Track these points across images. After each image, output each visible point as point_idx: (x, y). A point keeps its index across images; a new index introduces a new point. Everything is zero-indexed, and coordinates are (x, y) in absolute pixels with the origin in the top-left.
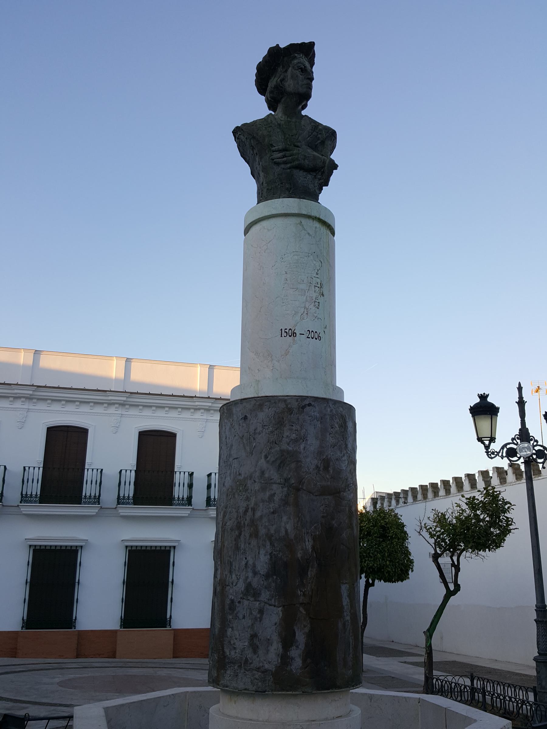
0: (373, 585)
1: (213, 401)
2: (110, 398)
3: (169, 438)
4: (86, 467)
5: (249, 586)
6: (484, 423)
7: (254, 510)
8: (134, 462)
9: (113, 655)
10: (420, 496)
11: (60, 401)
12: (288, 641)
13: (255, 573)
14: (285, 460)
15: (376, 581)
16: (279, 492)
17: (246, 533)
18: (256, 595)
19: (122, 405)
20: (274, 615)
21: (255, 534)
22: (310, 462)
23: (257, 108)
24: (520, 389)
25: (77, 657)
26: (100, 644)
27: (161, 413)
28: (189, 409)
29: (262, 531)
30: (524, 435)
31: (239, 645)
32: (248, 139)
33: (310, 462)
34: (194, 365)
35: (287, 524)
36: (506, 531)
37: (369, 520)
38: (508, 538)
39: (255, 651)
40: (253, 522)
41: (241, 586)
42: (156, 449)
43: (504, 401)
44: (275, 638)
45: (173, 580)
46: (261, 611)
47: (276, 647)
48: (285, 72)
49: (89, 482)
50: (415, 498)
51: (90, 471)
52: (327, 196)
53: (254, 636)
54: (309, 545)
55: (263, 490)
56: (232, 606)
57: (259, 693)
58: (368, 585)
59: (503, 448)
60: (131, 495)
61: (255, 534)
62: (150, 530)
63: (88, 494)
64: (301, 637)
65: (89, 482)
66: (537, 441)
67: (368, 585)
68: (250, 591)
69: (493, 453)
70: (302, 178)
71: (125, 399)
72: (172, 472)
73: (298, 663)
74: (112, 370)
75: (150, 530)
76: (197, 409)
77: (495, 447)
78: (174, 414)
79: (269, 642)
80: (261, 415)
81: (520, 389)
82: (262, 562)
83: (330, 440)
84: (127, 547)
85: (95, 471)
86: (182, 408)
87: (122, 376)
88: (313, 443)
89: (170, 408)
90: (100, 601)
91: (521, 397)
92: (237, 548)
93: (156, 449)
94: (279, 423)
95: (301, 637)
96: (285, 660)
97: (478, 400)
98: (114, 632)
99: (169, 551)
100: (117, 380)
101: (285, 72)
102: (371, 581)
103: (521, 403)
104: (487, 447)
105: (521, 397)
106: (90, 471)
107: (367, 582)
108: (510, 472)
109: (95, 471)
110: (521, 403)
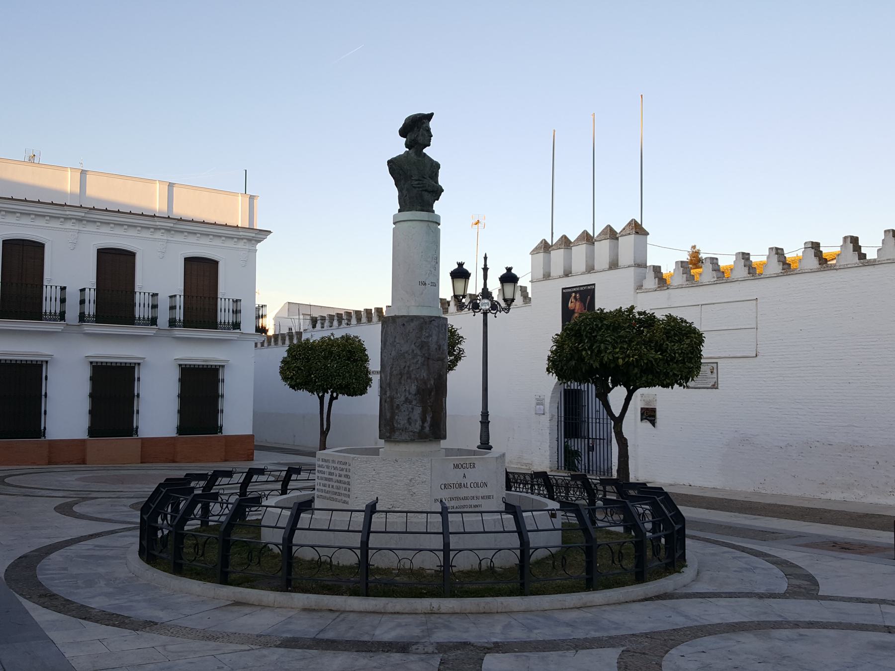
0: (336, 398)
1: (174, 221)
2: (68, 213)
3: (128, 257)
4: (45, 283)
5: (407, 399)
6: (460, 283)
7: (409, 367)
8: (94, 280)
9: (84, 462)
10: (364, 319)
11: (15, 213)
12: (424, 420)
13: (410, 394)
14: (423, 345)
15: (340, 395)
16: (420, 359)
17: (405, 377)
18: (410, 402)
19: (80, 220)
20: (418, 411)
21: (410, 377)
22: (433, 346)
23: (399, 147)
24: (486, 258)
25: (50, 463)
26: (68, 454)
27: (119, 231)
28: (149, 228)
29: (413, 376)
31: (402, 422)
32: (396, 167)
33: (433, 346)
34: (153, 181)
35: (424, 374)
36: (458, 358)
37: (339, 346)
38: (459, 363)
39: (410, 424)
40: (408, 372)
41: (403, 398)
42: (116, 267)
43: (473, 267)
44: (419, 419)
45: (46, 393)
46: (413, 409)
47: (419, 422)
48: (416, 129)
49: (48, 299)
50: (359, 320)
51: (49, 287)
52: (437, 206)
53: (409, 419)
54: (432, 382)
55: (413, 358)
56: (398, 407)
57: (412, 441)
58: (332, 399)
60: (182, 319)
61: (410, 377)
62: (115, 348)
63: (48, 311)
64: (429, 419)
65: (48, 299)
67: (332, 399)
68: (407, 400)
70: (426, 196)
71: (83, 214)
72: (133, 293)
73: (427, 429)
74: (68, 184)
75: (115, 348)
76: (157, 229)
78: (132, 232)
79: (416, 421)
80: (412, 324)
81: (486, 258)
82: (413, 389)
83: (441, 336)
84: (91, 363)
85: (54, 288)
86: (129, 226)
87: (78, 190)
88: (435, 338)
89: (129, 226)
90: (157, 411)
91: (485, 265)
92: (400, 383)
93: (116, 267)
94: (421, 329)
95: (429, 419)
96: (423, 427)
97: (457, 266)
98: (84, 441)
99: (41, 366)
100: (72, 194)
101: (416, 129)
102: (335, 395)
103: (485, 269)
105: (485, 265)
106: (49, 287)
107: (332, 395)
108: (452, 304)
109: (54, 288)
110: (485, 269)
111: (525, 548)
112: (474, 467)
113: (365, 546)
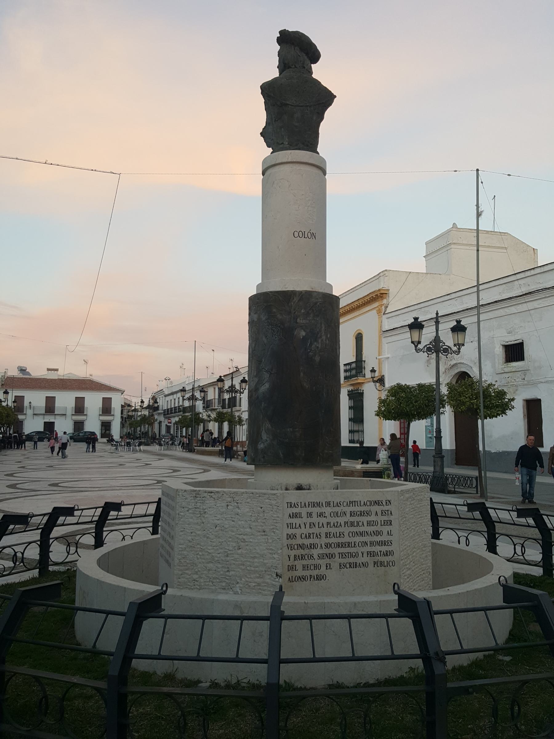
30: (437, 340)
48: (297, 50)
59: (424, 347)
66: (444, 343)
69: (419, 350)
77: (420, 346)
101: (297, 50)
104: (416, 346)
111: (429, 653)
112: (391, 524)
113: (274, 659)
